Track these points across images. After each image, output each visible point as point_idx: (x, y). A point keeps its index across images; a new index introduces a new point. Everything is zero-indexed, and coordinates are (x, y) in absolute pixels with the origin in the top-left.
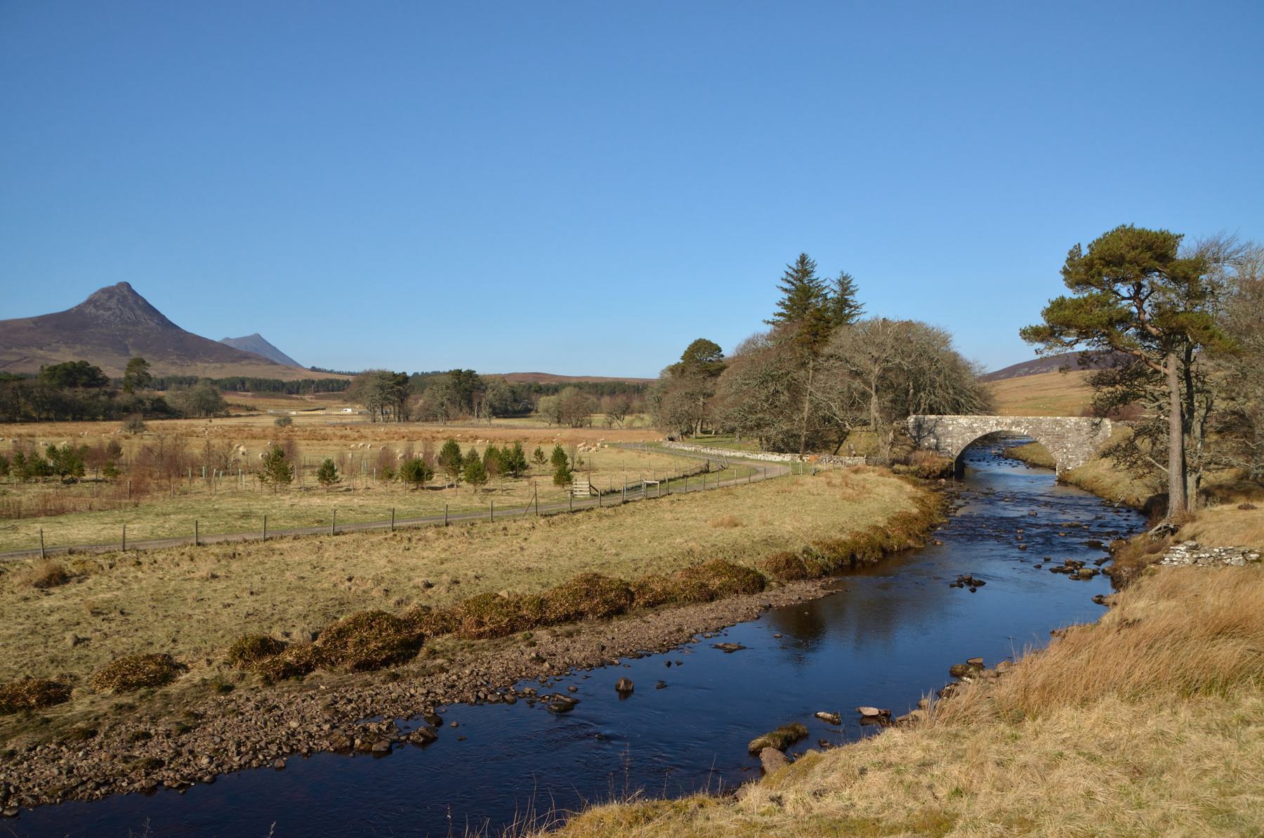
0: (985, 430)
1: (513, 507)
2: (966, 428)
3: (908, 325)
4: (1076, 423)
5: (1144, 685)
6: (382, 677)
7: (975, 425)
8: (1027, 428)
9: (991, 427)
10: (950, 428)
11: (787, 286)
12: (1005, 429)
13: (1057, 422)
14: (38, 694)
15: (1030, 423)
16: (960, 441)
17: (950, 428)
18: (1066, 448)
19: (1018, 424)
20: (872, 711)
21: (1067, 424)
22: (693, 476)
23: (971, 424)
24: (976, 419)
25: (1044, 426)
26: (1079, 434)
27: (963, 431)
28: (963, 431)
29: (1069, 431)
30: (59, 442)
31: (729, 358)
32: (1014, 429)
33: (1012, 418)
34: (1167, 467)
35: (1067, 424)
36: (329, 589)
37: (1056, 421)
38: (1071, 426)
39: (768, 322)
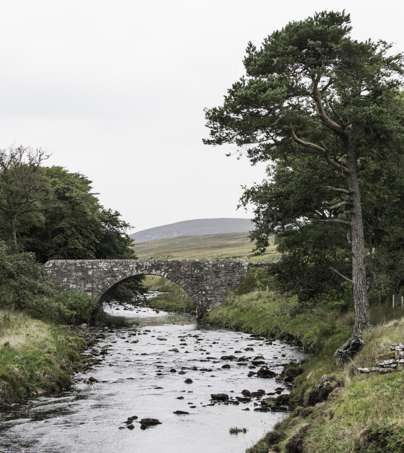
0: (125, 274)
1: (178, 251)
2: (106, 273)
5: (363, 447)
7: (115, 269)
9: (132, 271)
10: (90, 273)
14: (269, 80)
16: (100, 287)
17: (90, 273)
18: (205, 290)
21: (205, 266)
23: (112, 268)
24: (117, 263)
27: (103, 275)
28: (103, 275)
29: (208, 273)
34: (351, 279)
35: (205, 266)
38: (209, 268)
39: (344, 11)
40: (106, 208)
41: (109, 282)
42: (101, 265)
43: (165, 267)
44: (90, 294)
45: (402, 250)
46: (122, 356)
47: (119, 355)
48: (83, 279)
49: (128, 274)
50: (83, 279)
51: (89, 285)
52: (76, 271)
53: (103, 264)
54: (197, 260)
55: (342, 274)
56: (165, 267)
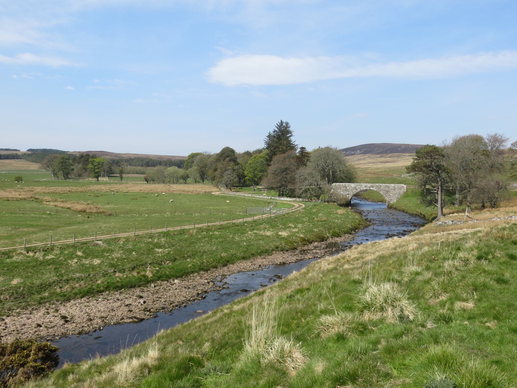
3: (328, 148)
4: (393, 187)
6: (408, 380)
8: (376, 188)
10: (348, 188)
11: (279, 124)
12: (368, 188)
13: (387, 186)
15: (377, 186)
17: (348, 188)
19: (373, 187)
20: (200, 311)
22: (400, 211)
25: (382, 188)
26: (395, 191)
29: (391, 189)
30: (408, 243)
31: (239, 154)
32: (371, 188)
33: (370, 184)
36: (220, 350)
37: (386, 186)
40: (253, 151)
41: (355, 192)
42: (352, 185)
43: (375, 187)
44: (348, 196)
45: (9, 340)
46: (61, 324)
47: (141, 294)
48: (345, 190)
49: (362, 189)
50: (345, 190)
51: (348, 192)
52: (343, 187)
53: (353, 185)
54: (132, 157)
55: (230, 198)
56: (375, 187)
